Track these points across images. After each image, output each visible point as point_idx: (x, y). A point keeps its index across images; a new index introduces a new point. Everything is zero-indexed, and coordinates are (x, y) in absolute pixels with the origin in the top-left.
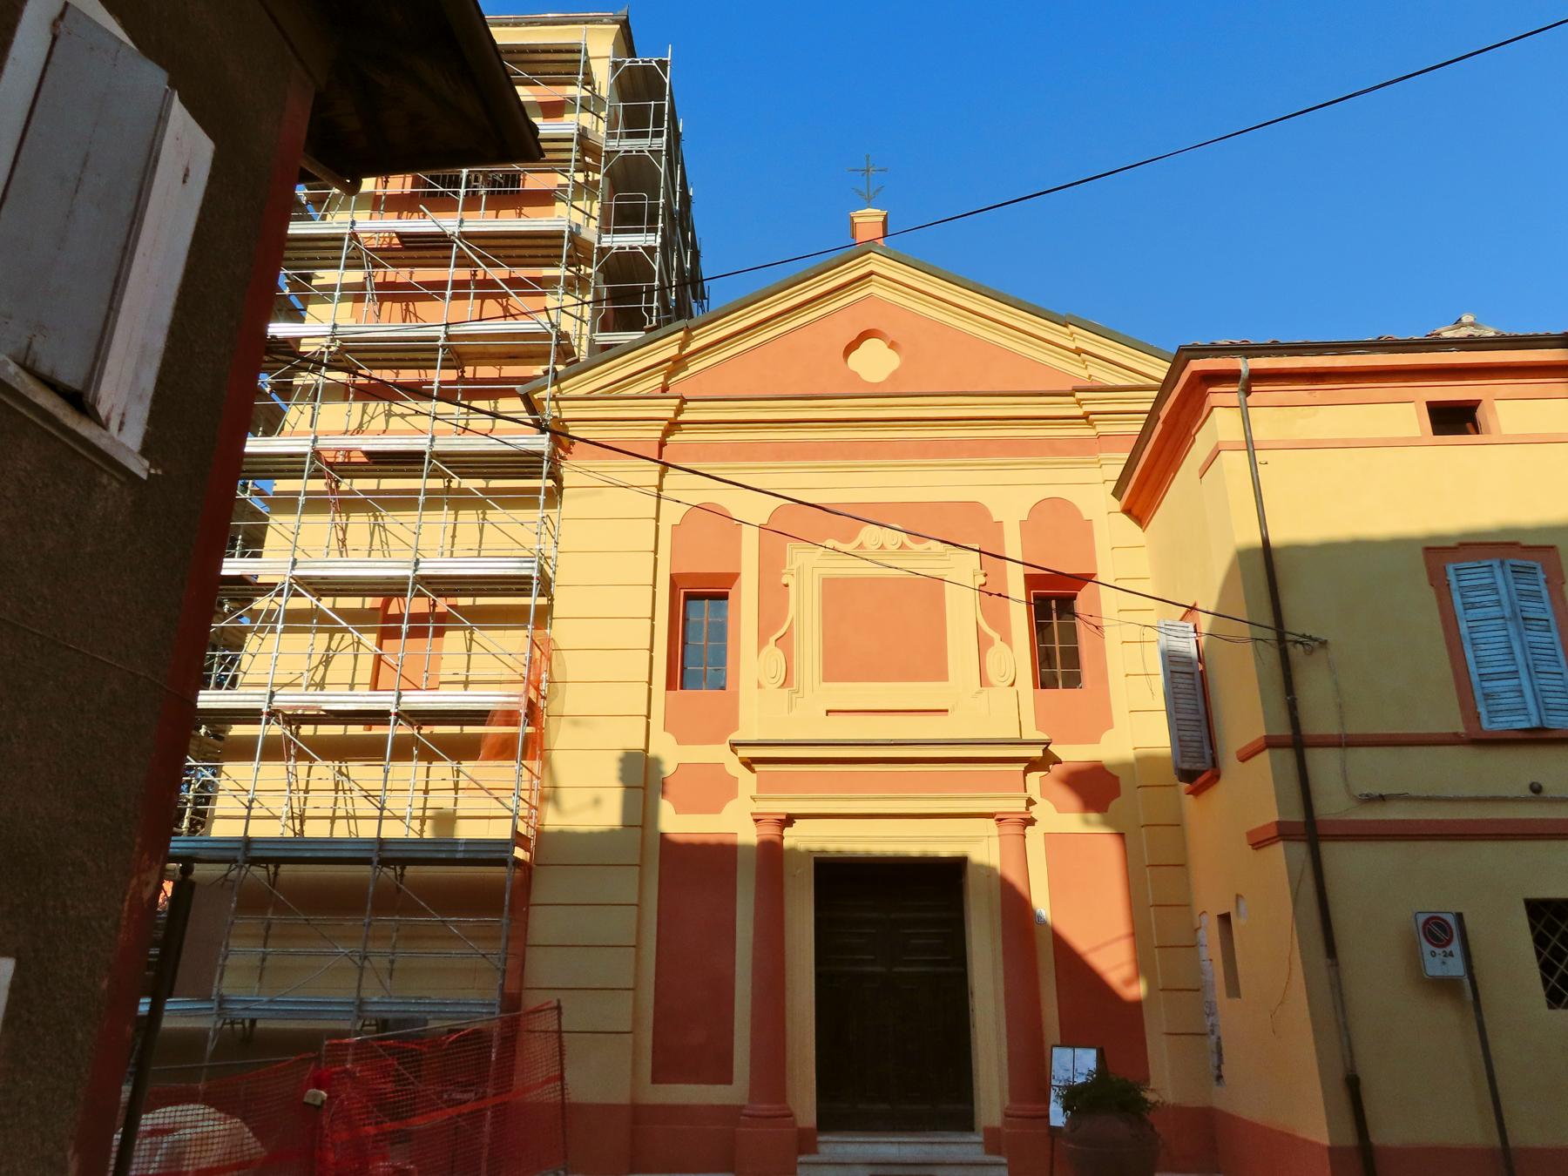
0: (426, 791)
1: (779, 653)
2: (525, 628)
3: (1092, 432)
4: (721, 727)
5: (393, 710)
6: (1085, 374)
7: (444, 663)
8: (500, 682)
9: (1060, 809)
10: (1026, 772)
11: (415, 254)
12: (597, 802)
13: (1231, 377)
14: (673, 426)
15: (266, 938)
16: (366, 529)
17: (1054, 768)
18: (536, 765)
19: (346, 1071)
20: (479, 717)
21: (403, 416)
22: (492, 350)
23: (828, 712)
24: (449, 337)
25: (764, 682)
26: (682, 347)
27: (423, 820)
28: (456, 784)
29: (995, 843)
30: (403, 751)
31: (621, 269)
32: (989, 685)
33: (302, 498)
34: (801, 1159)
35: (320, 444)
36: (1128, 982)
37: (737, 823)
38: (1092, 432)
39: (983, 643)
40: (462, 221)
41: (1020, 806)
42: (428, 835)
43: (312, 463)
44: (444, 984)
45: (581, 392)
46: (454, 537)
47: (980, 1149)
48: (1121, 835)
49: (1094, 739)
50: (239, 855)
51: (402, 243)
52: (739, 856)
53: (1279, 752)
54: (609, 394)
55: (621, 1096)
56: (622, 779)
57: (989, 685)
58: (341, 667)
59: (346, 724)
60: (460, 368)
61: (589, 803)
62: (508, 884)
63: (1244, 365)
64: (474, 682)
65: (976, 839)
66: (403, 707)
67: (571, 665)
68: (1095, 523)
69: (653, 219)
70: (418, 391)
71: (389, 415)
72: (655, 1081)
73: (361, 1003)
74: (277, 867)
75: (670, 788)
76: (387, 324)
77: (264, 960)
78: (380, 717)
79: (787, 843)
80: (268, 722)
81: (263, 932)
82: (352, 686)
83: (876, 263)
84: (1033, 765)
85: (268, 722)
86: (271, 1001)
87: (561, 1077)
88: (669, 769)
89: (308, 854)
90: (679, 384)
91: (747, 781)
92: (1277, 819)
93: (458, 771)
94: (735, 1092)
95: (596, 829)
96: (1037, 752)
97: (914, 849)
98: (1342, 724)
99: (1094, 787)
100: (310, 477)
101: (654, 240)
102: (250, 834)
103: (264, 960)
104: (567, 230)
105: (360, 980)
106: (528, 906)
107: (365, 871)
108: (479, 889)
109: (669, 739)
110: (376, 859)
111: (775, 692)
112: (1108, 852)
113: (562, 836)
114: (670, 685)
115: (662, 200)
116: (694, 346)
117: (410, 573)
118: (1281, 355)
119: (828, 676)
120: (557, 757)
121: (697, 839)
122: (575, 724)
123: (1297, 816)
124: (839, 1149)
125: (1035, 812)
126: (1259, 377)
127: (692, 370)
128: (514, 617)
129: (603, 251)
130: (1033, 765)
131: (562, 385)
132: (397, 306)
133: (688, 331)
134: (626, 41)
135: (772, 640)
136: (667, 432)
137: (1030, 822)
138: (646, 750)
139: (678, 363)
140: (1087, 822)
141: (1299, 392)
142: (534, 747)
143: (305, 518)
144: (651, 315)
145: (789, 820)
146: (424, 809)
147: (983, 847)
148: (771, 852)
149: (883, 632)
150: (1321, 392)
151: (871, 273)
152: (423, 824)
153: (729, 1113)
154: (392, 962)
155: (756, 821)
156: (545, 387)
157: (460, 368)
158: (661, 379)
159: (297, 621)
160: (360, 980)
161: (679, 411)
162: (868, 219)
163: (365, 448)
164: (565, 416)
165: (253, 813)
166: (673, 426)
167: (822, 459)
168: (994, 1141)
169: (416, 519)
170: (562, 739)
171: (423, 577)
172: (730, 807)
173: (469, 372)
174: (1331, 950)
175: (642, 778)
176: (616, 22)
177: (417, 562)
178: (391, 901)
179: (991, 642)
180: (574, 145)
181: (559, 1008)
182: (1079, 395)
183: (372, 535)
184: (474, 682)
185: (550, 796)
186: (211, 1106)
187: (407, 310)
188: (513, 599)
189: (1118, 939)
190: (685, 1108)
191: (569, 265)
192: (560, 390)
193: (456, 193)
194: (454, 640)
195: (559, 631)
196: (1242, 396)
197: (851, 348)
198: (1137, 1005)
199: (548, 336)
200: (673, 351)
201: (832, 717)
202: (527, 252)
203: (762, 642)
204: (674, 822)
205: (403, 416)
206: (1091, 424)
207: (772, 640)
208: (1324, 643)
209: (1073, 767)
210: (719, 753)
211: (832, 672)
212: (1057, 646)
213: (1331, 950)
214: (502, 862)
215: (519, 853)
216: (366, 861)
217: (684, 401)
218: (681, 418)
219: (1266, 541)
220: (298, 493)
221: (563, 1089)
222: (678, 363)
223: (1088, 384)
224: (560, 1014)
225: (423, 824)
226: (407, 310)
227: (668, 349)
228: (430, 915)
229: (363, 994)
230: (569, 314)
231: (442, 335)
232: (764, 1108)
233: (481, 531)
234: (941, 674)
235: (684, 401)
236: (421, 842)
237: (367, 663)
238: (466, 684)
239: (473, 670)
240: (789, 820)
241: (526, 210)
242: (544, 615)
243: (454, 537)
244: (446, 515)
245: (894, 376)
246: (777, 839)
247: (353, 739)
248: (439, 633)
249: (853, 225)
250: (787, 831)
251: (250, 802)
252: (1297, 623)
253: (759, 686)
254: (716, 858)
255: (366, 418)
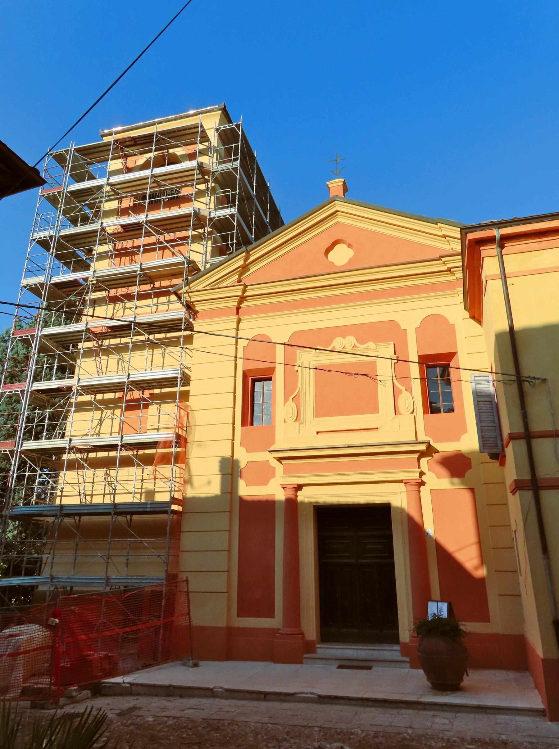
0: (142, 480)
1: (294, 405)
2: (175, 402)
3: (454, 278)
4: (266, 442)
5: (120, 444)
6: (449, 247)
7: (149, 421)
8: (167, 428)
9: (439, 477)
10: (419, 459)
11: (131, 233)
12: (209, 483)
13: (490, 240)
14: (243, 299)
15: (76, 550)
16: (115, 361)
17: (436, 456)
18: (183, 466)
19: (71, 610)
20: (153, 445)
21: (130, 308)
22: (163, 273)
23: (317, 433)
24: (142, 270)
25: (287, 420)
26: (245, 260)
27: (141, 493)
28: (155, 477)
29: (405, 495)
30: (126, 462)
31: (222, 225)
32: (400, 414)
33: (130, 345)
34: (305, 656)
35: (89, 326)
36: (476, 568)
37: (275, 490)
38: (454, 278)
39: (396, 393)
40: (147, 215)
41: (416, 476)
42: (143, 501)
43: (86, 335)
44: (144, 569)
45: (200, 287)
46: (152, 361)
47: (398, 654)
48: (472, 490)
49: (457, 439)
50: (58, 513)
51: (124, 229)
52: (277, 505)
53: (518, 442)
54: (214, 286)
55: (222, 623)
56: (221, 471)
57: (400, 414)
58: (107, 424)
59: (109, 451)
60: (152, 282)
61: (206, 483)
62: (169, 523)
63: (496, 233)
64: (162, 429)
65: (394, 494)
66: (124, 442)
67: (198, 418)
68: (456, 326)
69: (233, 201)
70: (129, 297)
71: (124, 308)
72: (239, 616)
73: (108, 579)
74: (131, 517)
75: (243, 474)
76: (125, 267)
77: (75, 559)
78: (113, 447)
79: (300, 499)
80: (121, 450)
81: (75, 547)
82: (111, 434)
83: (339, 206)
84: (422, 454)
85: (69, 453)
86: (68, 578)
87: (189, 614)
88: (243, 465)
89: (86, 511)
90: (247, 278)
91: (279, 468)
92: (515, 478)
93: (156, 470)
94: (275, 622)
95: (209, 495)
96: (423, 447)
97: (363, 500)
98: (554, 424)
99: (456, 465)
100: (85, 341)
101: (233, 211)
102: (63, 503)
103: (75, 559)
104: (192, 212)
105: (107, 568)
106: (180, 532)
107: (107, 518)
108: (151, 525)
109: (243, 450)
110: (113, 513)
111: (294, 424)
112: (465, 498)
113: (194, 499)
114: (244, 424)
115: (238, 191)
116: (251, 259)
117: (126, 380)
118: (519, 225)
119: (318, 414)
120: (192, 462)
121: (256, 498)
122: (199, 446)
123: (527, 476)
124: (327, 651)
125: (424, 478)
126: (505, 239)
127: (252, 271)
128: (171, 397)
129: (211, 219)
130: (422, 454)
131: (191, 285)
132: (127, 258)
133: (248, 252)
134: (226, 116)
135: (291, 398)
136: (240, 302)
137: (422, 483)
138: (232, 456)
139: (245, 268)
140: (452, 483)
141: (533, 244)
142: (180, 459)
143: (82, 360)
144: (233, 247)
145: (299, 487)
146: (142, 488)
147: (398, 498)
148: (292, 504)
149: (348, 388)
150: (545, 242)
151: (337, 211)
152: (141, 496)
153: (272, 632)
154: (128, 560)
155: (284, 488)
156: (182, 288)
157: (152, 282)
158: (237, 277)
159: (83, 407)
160: (107, 568)
161: (244, 291)
162: (336, 184)
163: (107, 325)
164: (192, 300)
165: (64, 494)
166: (243, 299)
167: (284, 311)
168: (406, 650)
169: (128, 356)
170: (194, 453)
171: (133, 382)
172: (272, 482)
173: (157, 284)
174: (545, 549)
175: (230, 470)
176: (219, 110)
177: (129, 375)
178: (119, 532)
179: (401, 392)
180: (197, 172)
181: (187, 581)
182: (443, 259)
183: (118, 364)
184: (162, 429)
185: (188, 481)
186: (36, 624)
187: (132, 259)
188: (172, 389)
189: (471, 545)
190: (251, 629)
191: (194, 230)
192: (190, 288)
193: (145, 203)
194: (153, 409)
195: (193, 402)
196: (499, 250)
197: (328, 251)
198: (482, 580)
199: (183, 263)
200: (241, 262)
201: (319, 434)
202: (179, 225)
203: (286, 400)
204: (246, 490)
205: (130, 308)
206: (452, 273)
207: (291, 398)
208: (544, 380)
209: (445, 454)
210: (264, 456)
211: (320, 412)
212: (440, 391)
213: (545, 549)
214: (166, 512)
215: (174, 507)
216: (108, 514)
217: (246, 286)
218: (245, 295)
219: (511, 328)
220: (129, 343)
221: (190, 620)
222: (245, 268)
223: (451, 252)
224: (187, 583)
225: (141, 496)
226: (132, 259)
227: (239, 262)
228: (136, 538)
229: (109, 574)
230: (199, 252)
231: (139, 269)
232: (288, 630)
233: (164, 358)
234: (375, 410)
235: (246, 286)
236: (140, 504)
237: (117, 422)
238: (158, 429)
239: (157, 424)
240: (299, 487)
241: (182, 205)
242: (185, 396)
243: (152, 361)
244: (148, 352)
245: (350, 261)
246: (293, 497)
247: (103, 458)
248: (146, 406)
249: (329, 188)
250: (299, 493)
251: (74, 488)
252: (526, 372)
253: (285, 422)
254: (265, 507)
255: (115, 311)
